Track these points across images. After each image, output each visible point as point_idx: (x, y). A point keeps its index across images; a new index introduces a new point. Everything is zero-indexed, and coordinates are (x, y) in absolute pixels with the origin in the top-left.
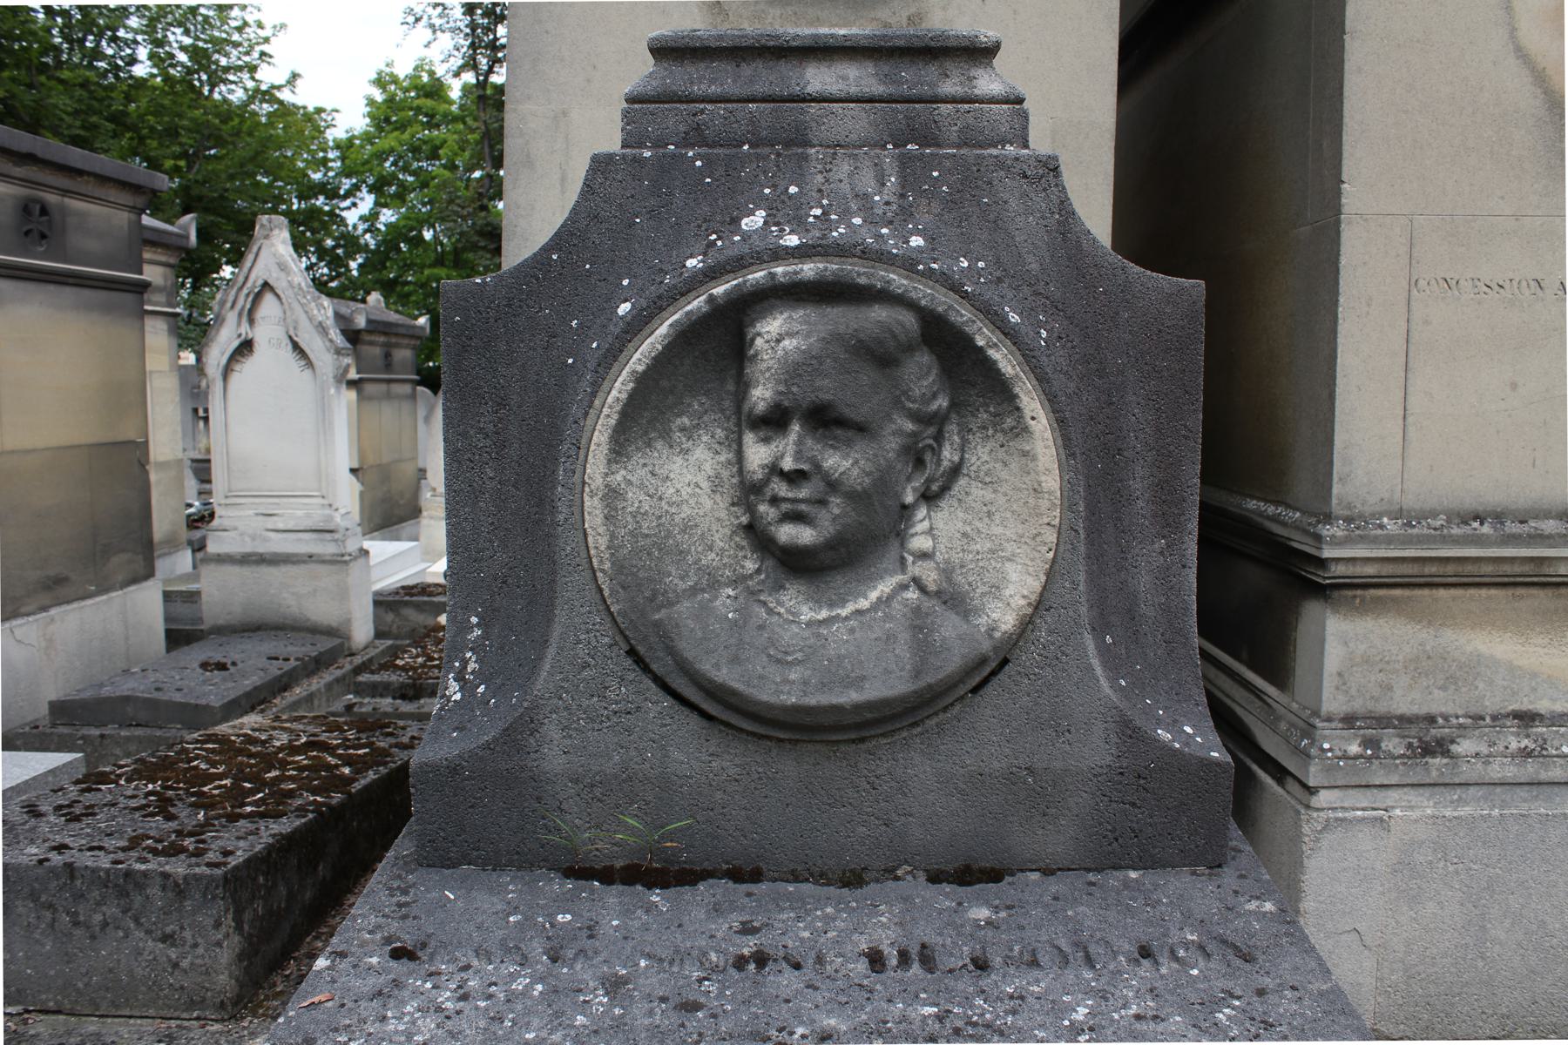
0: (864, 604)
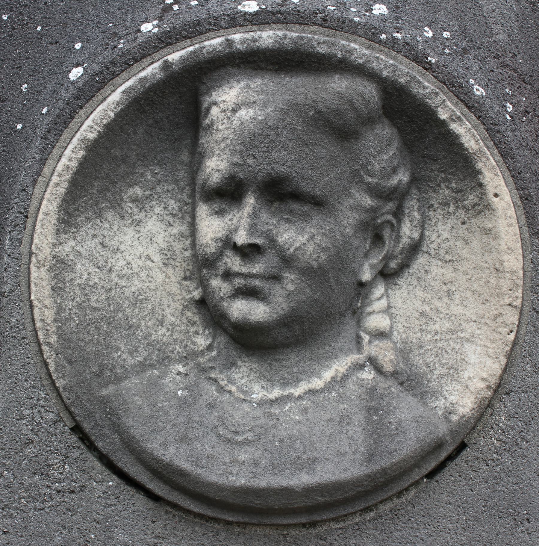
0: (317, 383)
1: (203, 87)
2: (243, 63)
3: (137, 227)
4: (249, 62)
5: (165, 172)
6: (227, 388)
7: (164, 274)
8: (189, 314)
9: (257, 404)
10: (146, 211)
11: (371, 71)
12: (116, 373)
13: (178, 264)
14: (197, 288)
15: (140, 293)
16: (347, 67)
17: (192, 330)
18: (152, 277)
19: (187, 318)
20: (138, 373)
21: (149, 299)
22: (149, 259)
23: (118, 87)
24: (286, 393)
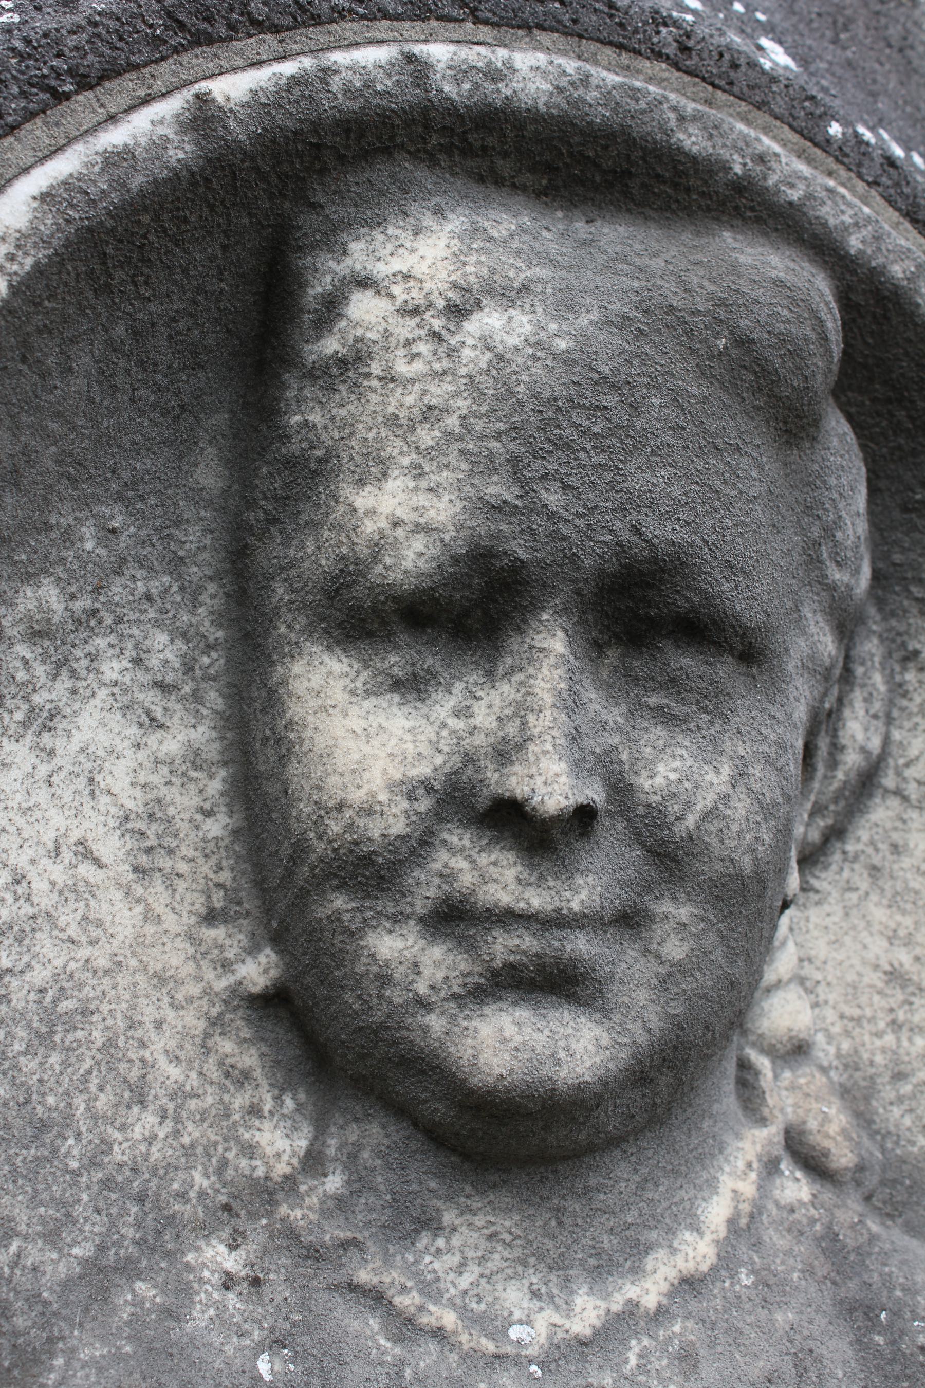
0: (697, 1251)
1: (308, 221)
2: (448, 149)
3: (46, 735)
4: (467, 151)
5: (140, 528)
6: (424, 1319)
7: (139, 909)
8: (227, 1046)
9: (542, 1365)
10: (74, 674)
11: (819, 230)
12: (16, 1334)
13: (183, 867)
14: (252, 950)
15: (62, 988)
16: (752, 209)
17: (239, 1101)
18: (99, 924)
19: (221, 1064)
20: (87, 1310)
21: (92, 1007)
22: (85, 857)
23: (16, 177)
24: (616, 1307)
